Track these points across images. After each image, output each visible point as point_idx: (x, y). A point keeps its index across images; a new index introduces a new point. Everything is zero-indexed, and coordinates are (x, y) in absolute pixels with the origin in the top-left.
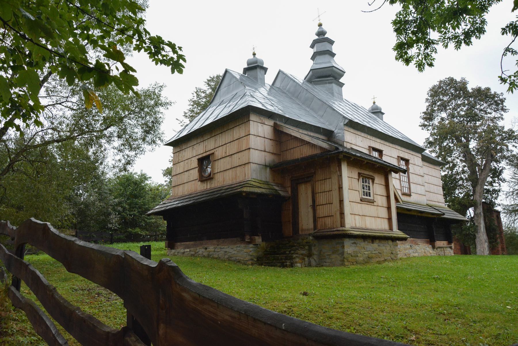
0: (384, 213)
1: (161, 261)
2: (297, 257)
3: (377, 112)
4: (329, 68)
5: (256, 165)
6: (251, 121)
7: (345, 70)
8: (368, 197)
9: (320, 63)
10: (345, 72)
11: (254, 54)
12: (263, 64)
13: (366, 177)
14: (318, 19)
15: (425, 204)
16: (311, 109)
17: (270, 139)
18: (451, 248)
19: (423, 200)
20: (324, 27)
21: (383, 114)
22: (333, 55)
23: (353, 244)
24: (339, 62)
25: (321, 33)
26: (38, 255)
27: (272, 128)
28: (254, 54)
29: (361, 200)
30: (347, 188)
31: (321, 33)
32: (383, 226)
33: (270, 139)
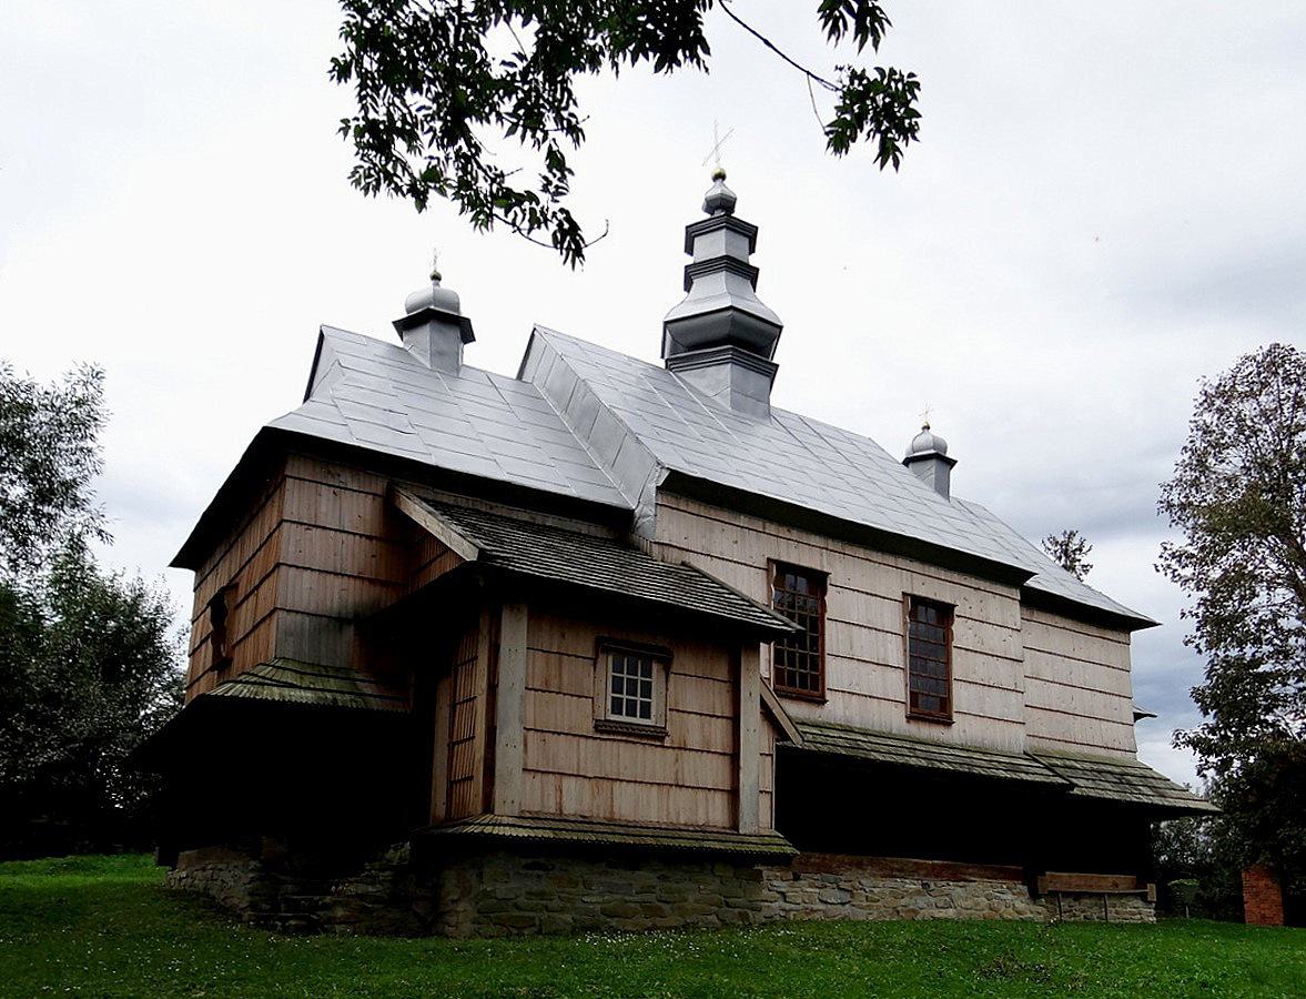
0: (712, 771)
1: (1285, 924)
2: (335, 902)
3: (934, 460)
4: (713, 316)
5: (299, 616)
6: (289, 481)
7: (783, 321)
8: (638, 720)
9: (707, 299)
10: (781, 328)
11: (436, 278)
12: (456, 307)
13: (624, 654)
14: (714, 157)
15: (1019, 750)
16: (592, 444)
17: (368, 537)
18: (1143, 897)
19: (1013, 739)
20: (732, 186)
21: (951, 463)
22: (751, 274)
23: (527, 867)
24: (769, 298)
25: (722, 207)
26: (153, 885)
27: (379, 500)
28: (436, 278)
29: (597, 729)
30: (519, 688)
31: (722, 207)
32: (701, 812)
33: (368, 537)
